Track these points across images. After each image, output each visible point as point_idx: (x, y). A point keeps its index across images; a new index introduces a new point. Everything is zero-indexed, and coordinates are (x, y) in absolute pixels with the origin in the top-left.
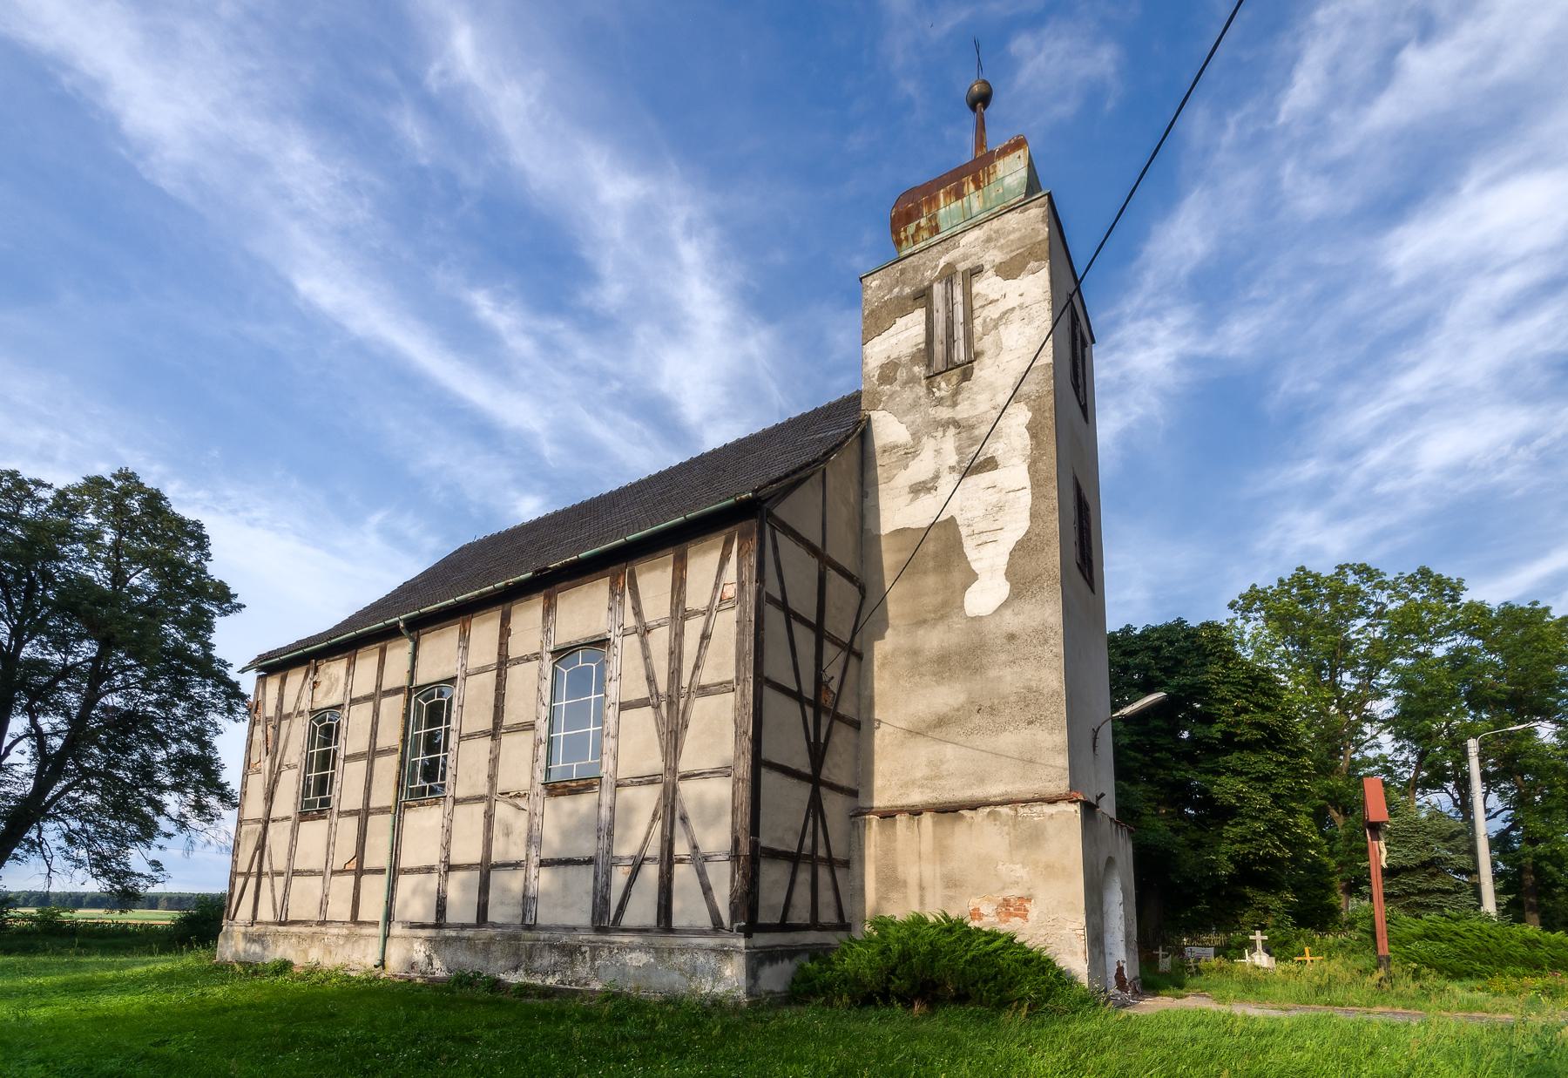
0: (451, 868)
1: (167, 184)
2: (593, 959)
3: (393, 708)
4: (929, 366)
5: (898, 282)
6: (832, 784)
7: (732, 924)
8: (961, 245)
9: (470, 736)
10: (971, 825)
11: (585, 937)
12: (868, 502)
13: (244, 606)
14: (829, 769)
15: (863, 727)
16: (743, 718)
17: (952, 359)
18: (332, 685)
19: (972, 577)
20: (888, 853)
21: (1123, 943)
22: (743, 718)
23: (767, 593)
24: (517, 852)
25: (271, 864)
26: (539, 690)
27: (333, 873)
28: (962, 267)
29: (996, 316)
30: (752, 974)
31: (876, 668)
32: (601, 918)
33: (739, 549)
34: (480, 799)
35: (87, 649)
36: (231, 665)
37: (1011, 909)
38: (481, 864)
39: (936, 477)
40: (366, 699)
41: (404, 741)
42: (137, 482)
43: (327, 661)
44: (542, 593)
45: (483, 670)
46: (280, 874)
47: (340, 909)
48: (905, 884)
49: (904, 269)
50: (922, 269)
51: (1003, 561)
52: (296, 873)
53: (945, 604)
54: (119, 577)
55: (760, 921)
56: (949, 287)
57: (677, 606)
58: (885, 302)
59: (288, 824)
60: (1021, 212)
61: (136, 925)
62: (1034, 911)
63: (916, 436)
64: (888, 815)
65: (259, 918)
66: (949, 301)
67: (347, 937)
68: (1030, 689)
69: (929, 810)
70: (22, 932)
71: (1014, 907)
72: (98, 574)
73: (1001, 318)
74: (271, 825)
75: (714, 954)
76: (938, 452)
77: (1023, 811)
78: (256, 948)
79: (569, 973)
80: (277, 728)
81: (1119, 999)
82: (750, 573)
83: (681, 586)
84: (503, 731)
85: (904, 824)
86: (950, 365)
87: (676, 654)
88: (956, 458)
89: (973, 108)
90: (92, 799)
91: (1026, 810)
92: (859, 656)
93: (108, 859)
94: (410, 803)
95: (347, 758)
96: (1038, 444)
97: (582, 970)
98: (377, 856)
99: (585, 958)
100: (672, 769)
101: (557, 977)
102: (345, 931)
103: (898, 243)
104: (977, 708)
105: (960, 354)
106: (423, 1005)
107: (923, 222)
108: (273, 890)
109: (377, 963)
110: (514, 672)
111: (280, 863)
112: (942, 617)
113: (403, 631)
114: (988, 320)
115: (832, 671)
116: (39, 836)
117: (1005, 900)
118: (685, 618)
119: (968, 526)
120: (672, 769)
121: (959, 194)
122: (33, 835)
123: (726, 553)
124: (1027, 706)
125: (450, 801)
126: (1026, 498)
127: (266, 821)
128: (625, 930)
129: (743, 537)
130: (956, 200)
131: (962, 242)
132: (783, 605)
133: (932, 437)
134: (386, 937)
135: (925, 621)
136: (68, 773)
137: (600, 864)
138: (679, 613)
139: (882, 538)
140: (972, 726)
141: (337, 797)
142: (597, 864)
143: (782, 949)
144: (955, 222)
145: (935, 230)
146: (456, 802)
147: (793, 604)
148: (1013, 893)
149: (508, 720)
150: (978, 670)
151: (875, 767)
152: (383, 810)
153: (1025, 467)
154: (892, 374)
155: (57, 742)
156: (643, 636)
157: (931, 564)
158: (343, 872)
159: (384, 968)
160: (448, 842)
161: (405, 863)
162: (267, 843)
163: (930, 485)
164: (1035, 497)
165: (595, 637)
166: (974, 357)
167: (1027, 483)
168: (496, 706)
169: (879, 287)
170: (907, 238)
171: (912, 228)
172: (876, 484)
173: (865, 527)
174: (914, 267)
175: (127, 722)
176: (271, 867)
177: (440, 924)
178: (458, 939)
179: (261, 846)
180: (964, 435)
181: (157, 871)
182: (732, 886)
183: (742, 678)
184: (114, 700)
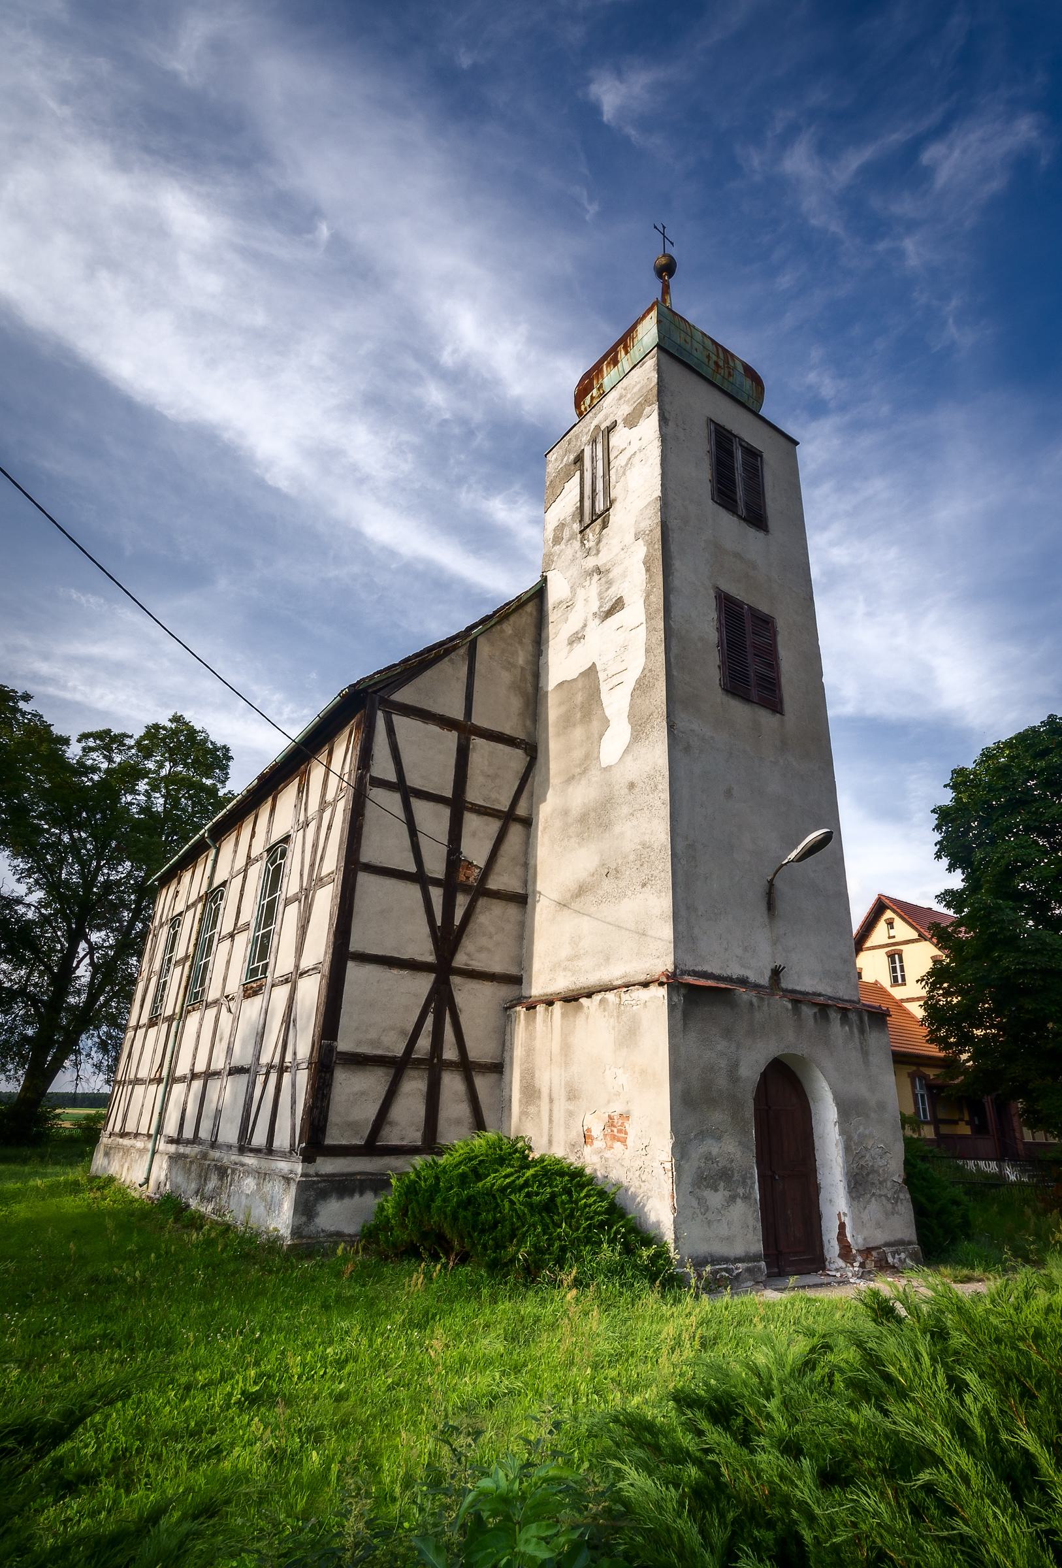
1: (283, 484)
6: (473, 971)
14: (468, 955)
15: (529, 900)
29: (623, 464)
30: (305, 1208)
31: (539, 833)
53: (587, 756)
55: (329, 1141)
59: (144, 1029)
62: (632, 1129)
66: (593, 459)
68: (644, 845)
69: (543, 1002)
73: (627, 464)
81: (838, 1275)
85: (542, 1013)
86: (595, 517)
88: (597, 604)
89: (660, 276)
92: (528, 823)
104: (606, 871)
105: (600, 506)
107: (595, 392)
115: (475, 849)
128: (252, 1150)
131: (605, 405)
132: (401, 787)
135: (573, 777)
140: (601, 893)
143: (363, 1178)
147: (414, 780)
148: (617, 1107)
151: (535, 948)
157: (579, 715)
163: (580, 635)
166: (610, 503)
167: (643, 618)
169: (556, 459)
171: (588, 400)
180: (603, 580)
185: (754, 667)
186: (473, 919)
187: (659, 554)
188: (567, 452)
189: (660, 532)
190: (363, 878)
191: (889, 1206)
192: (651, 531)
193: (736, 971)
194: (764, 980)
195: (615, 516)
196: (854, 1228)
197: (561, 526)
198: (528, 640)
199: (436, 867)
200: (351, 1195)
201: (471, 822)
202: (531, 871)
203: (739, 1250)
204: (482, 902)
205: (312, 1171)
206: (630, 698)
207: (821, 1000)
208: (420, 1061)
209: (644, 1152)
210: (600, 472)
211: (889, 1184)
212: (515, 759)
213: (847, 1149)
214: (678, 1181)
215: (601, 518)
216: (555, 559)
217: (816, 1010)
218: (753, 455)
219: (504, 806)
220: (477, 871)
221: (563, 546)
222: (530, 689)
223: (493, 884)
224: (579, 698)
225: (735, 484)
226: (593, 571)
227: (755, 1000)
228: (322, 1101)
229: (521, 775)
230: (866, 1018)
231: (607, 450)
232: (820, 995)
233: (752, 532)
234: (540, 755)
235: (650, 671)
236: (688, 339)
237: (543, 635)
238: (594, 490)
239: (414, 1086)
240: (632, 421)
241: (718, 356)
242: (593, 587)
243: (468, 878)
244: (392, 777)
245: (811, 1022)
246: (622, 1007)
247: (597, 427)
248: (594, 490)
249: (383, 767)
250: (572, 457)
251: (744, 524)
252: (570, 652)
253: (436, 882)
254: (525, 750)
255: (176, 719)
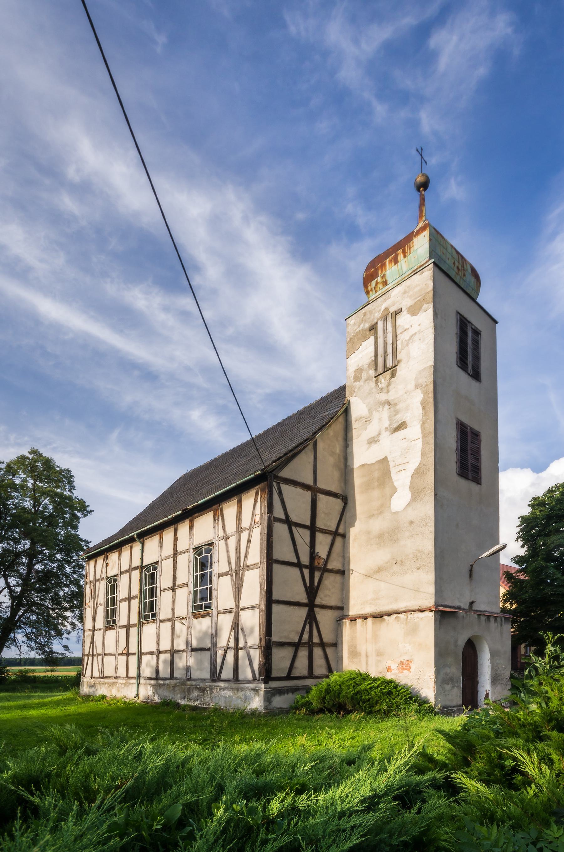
0: (160, 652)
2: (211, 694)
3: (136, 574)
4: (376, 370)
5: (362, 321)
7: (259, 677)
8: (392, 297)
9: (165, 590)
10: (388, 624)
11: (208, 684)
12: (349, 450)
13: (93, 511)
14: (321, 598)
15: (346, 573)
16: (262, 581)
17: (386, 367)
18: (114, 565)
19: (394, 490)
20: (353, 638)
21: (490, 680)
22: (262, 581)
23: (274, 517)
24: (182, 646)
25: (96, 650)
26: (189, 568)
27: (119, 654)
28: (392, 310)
29: (407, 338)
32: (213, 676)
33: (261, 497)
34: (169, 620)
35: (26, 544)
36: (90, 542)
37: (404, 666)
38: (170, 651)
39: (379, 434)
40: (126, 571)
41: (140, 592)
42: (39, 454)
43: (111, 553)
44: (189, 519)
45: (168, 558)
46: (100, 655)
47: (122, 672)
48: (360, 654)
49: (366, 312)
50: (373, 312)
51: (408, 481)
52: (106, 655)
53: (382, 506)
54: (37, 503)
55: (273, 676)
56: (385, 323)
57: (238, 526)
58: (357, 333)
59: (102, 632)
60: (420, 274)
61: (62, 677)
62: (413, 666)
63: (370, 411)
64: (353, 620)
65: (94, 676)
66: (385, 331)
67: (125, 684)
68: (419, 551)
69: (359, 617)
70: (14, 681)
71: (404, 666)
72: (28, 504)
73: (410, 339)
74: (95, 632)
75: (252, 691)
76: (380, 419)
77: (410, 616)
78: (92, 690)
79: (202, 700)
80: (95, 586)
82: (265, 509)
83: (240, 516)
84: (176, 587)
87: (238, 550)
89: (418, 189)
90: (34, 618)
91: (411, 616)
92: (344, 536)
93: (44, 645)
94: (144, 622)
95: (121, 601)
96: (425, 413)
97: (207, 699)
98: (133, 648)
99: (208, 693)
100: (238, 606)
101: (199, 702)
102: (124, 681)
103: (368, 293)
104: (395, 562)
105: (390, 363)
106: (223, 714)
107: (379, 279)
108: (98, 663)
109: (135, 696)
110: (180, 558)
111: (100, 651)
112: (381, 513)
113: (136, 539)
114: (404, 341)
115: (322, 550)
116: (14, 637)
117: (401, 662)
118: (241, 532)
119: (393, 461)
120: (238, 606)
121: (396, 261)
122: (12, 636)
123: (256, 499)
124: (417, 560)
125: (158, 620)
126: (419, 443)
127: (94, 630)
128: (222, 681)
129: (263, 490)
130: (395, 265)
133: (377, 411)
134: (138, 684)
135: (373, 515)
136: (23, 606)
137: (212, 649)
138: (240, 530)
139: (355, 470)
141: (118, 619)
142: (211, 650)
144: (395, 278)
145: (385, 283)
146: (161, 621)
147: (294, 518)
148: (405, 658)
149: (178, 583)
150: (396, 541)
151: (350, 594)
152: (134, 625)
153: (419, 426)
154: (359, 376)
155: (18, 589)
156: (226, 541)
157: (376, 484)
158: (122, 654)
159: (138, 698)
160: (159, 640)
161: (144, 650)
162: (95, 641)
163: (376, 439)
164: (424, 443)
165: (208, 541)
167: (420, 436)
168: (173, 575)
169: (354, 324)
170: (372, 289)
171: (373, 283)
172: (352, 440)
173: (348, 464)
174: (370, 311)
175: (47, 575)
176: (97, 652)
177: (157, 678)
178: (164, 685)
179: (92, 642)
180: (392, 409)
181: (67, 650)
182: (259, 660)
183: (262, 561)
184: (38, 567)
185: (471, 460)
186: (322, 583)
187: (432, 400)
188: (362, 321)
189: (433, 388)
190: (275, 566)
191: (504, 687)
192: (427, 385)
193: (457, 604)
194: (467, 607)
195: (401, 371)
196: (492, 695)
197: (360, 370)
198: (341, 439)
199: (305, 559)
200: (284, 694)
201: (320, 537)
202: (347, 560)
203: (454, 703)
204: (326, 574)
205: (268, 687)
206: (410, 478)
207: (487, 614)
208: (305, 644)
209: (420, 673)
210: (390, 341)
211: (505, 679)
212: (337, 504)
213: (492, 668)
214: (437, 682)
215: (392, 371)
216: (356, 390)
217: (486, 617)
218: (477, 333)
219: (333, 529)
220: (323, 560)
221: (361, 382)
222: (342, 466)
223: (330, 566)
224: (376, 474)
225: (467, 353)
226: (385, 403)
227: (465, 616)
228: (269, 661)
229: (340, 512)
230: (503, 619)
231: (395, 327)
232: (486, 611)
233: (474, 383)
234: (349, 502)
235: (424, 465)
236: (445, 251)
237: (349, 435)
238: (385, 352)
239: (303, 654)
240: (414, 310)
241: (459, 262)
242: (385, 413)
243: (319, 564)
244: (283, 517)
245: (484, 622)
246: (409, 620)
247: (387, 309)
248: (385, 352)
249: (279, 513)
250: (367, 325)
251: (470, 378)
252: (368, 448)
253: (306, 567)
254: (342, 499)
255: (34, 452)
